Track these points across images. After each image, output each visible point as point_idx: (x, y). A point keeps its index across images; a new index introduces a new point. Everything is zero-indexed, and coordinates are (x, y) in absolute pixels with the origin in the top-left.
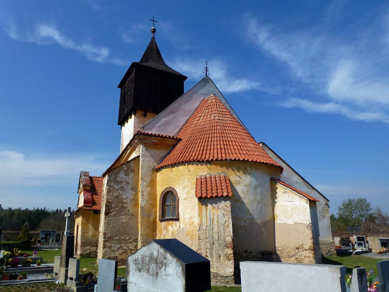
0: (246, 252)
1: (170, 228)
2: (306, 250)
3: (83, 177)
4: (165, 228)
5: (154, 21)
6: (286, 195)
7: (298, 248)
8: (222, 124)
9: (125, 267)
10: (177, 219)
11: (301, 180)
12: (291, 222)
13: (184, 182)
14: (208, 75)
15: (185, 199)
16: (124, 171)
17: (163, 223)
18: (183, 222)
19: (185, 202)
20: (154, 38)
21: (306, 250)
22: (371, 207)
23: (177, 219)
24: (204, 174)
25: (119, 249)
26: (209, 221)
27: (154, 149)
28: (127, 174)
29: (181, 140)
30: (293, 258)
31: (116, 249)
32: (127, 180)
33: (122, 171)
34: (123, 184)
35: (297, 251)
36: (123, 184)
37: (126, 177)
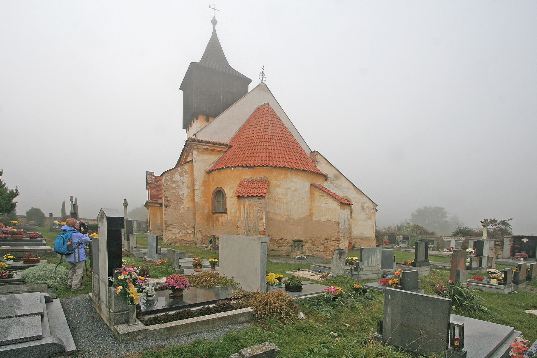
0: (281, 239)
1: (220, 219)
2: (333, 241)
3: (149, 176)
4: (217, 219)
5: (214, 9)
6: (322, 198)
7: (326, 239)
8: (270, 134)
9: (216, 260)
10: (225, 213)
11: (352, 187)
12: (323, 219)
13: (231, 184)
14: (264, 82)
15: (232, 197)
16: (179, 173)
17: (215, 215)
18: (230, 215)
19: (231, 199)
20: (214, 33)
21: (333, 241)
22: (447, 215)
23: (225, 213)
24: (248, 178)
25: (179, 232)
26: (246, 214)
27: (206, 154)
28: (182, 176)
29: (232, 147)
30: (322, 246)
31: (177, 232)
32: (182, 180)
33: (177, 173)
34: (179, 183)
35: (326, 241)
36: (179, 183)
37: (182, 178)
